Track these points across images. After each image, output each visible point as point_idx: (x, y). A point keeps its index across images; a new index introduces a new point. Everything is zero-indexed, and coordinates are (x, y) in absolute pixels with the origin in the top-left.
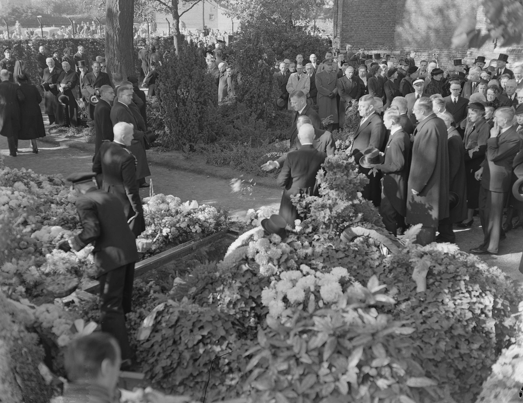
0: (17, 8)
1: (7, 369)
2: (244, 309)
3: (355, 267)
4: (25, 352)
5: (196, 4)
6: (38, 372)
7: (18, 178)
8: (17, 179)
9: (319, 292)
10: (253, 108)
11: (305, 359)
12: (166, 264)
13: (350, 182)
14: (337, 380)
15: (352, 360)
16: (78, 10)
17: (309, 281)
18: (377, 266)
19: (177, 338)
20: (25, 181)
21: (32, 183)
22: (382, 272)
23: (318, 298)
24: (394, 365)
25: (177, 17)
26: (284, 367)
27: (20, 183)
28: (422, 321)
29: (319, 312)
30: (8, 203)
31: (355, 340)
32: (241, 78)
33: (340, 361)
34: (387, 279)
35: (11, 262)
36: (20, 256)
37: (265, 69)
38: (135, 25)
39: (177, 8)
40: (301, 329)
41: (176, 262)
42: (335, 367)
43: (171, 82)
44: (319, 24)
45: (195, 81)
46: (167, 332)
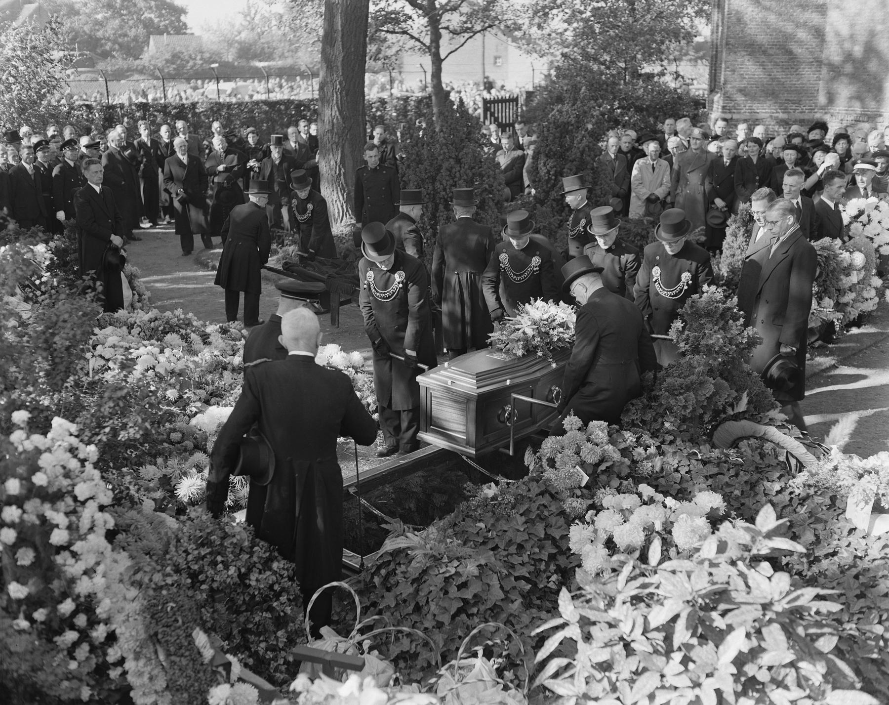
0: (179, 52)
1: (143, 636)
2: (537, 557)
3: (737, 492)
4: (172, 608)
5: (471, 37)
6: (191, 642)
7: (171, 327)
8: (170, 328)
9: (670, 532)
10: (563, 214)
11: (641, 645)
12: (409, 477)
13: (731, 341)
14: (697, 685)
15: (592, 279)
16: (278, 52)
17: (655, 516)
18: (778, 492)
19: (422, 602)
20: (183, 332)
21: (193, 336)
22: (788, 503)
23: (667, 543)
24: (802, 664)
25: (438, 62)
26: (603, 656)
27: (175, 335)
28: (858, 592)
29: (667, 565)
30: (153, 368)
31: (730, 614)
32: (545, 163)
33: (703, 653)
34: (795, 516)
35: (155, 464)
36: (170, 454)
37: (587, 146)
38: (368, 77)
39: (438, 47)
40: (634, 592)
41: (425, 474)
42: (694, 662)
43: (426, 169)
44: (685, 68)
45: (466, 167)
46: (406, 590)
